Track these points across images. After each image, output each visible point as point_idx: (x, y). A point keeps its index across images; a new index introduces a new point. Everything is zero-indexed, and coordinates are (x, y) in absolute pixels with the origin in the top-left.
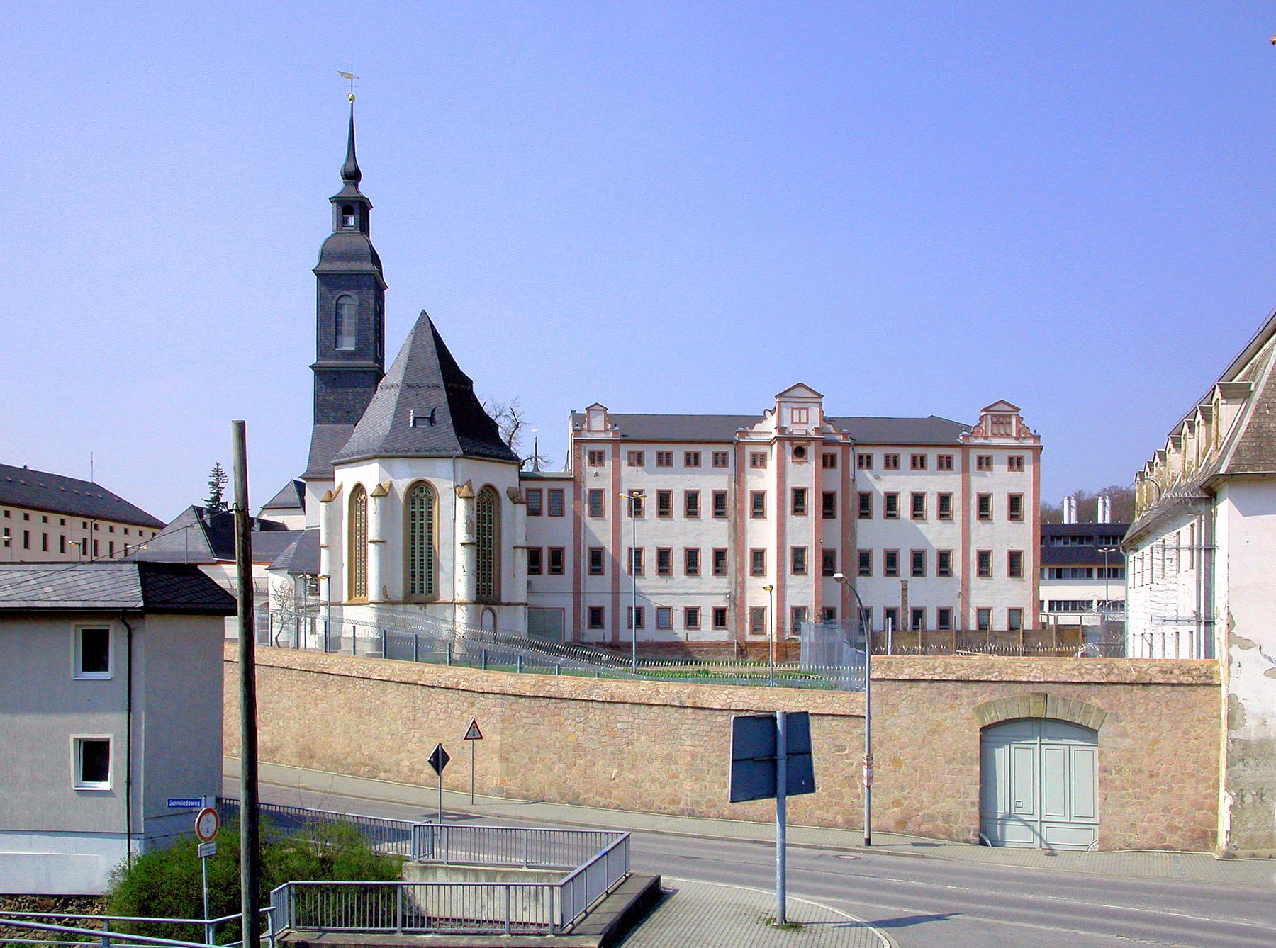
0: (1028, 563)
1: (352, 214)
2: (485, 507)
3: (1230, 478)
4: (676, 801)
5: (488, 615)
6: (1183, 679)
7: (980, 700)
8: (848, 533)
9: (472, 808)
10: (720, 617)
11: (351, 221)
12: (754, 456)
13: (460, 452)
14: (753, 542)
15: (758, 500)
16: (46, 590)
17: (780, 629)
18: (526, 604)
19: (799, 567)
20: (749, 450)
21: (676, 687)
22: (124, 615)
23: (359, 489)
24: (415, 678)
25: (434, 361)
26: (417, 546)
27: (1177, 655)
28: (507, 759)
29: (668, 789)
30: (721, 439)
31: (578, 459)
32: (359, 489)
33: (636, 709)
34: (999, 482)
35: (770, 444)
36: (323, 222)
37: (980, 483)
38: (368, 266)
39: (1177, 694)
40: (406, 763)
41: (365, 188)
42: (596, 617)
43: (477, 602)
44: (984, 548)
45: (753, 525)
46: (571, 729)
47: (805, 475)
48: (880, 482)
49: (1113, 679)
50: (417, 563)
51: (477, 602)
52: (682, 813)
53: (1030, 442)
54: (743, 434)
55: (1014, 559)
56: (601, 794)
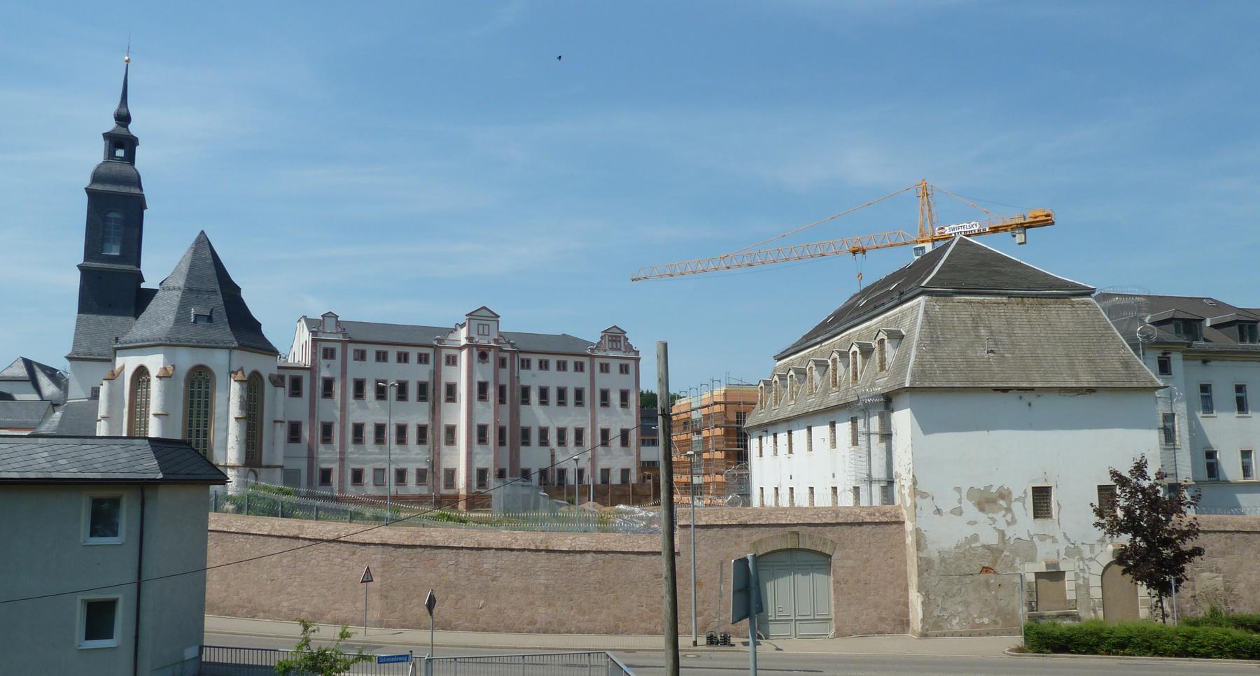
0: (633, 437)
3: (911, 390)
4: (532, 622)
5: (252, 474)
6: (884, 519)
7: (755, 538)
8: (515, 415)
9: (367, 639)
10: (421, 476)
11: (120, 153)
12: (448, 357)
13: (236, 344)
14: (447, 420)
15: (451, 391)
17: (469, 485)
18: (282, 467)
20: (444, 353)
22: (143, 486)
23: (141, 372)
24: (295, 532)
25: (212, 271)
28: (386, 597)
29: (526, 614)
31: (314, 354)
32: (141, 372)
33: (500, 553)
34: (614, 382)
36: (96, 154)
37: (602, 381)
40: (285, 604)
41: (133, 128)
42: (326, 476)
44: (604, 427)
45: (323, 403)
47: (485, 372)
48: (533, 378)
49: (840, 520)
50: (194, 433)
51: (245, 465)
52: (538, 631)
53: (632, 355)
54: (439, 341)
55: (625, 434)
56: (470, 621)
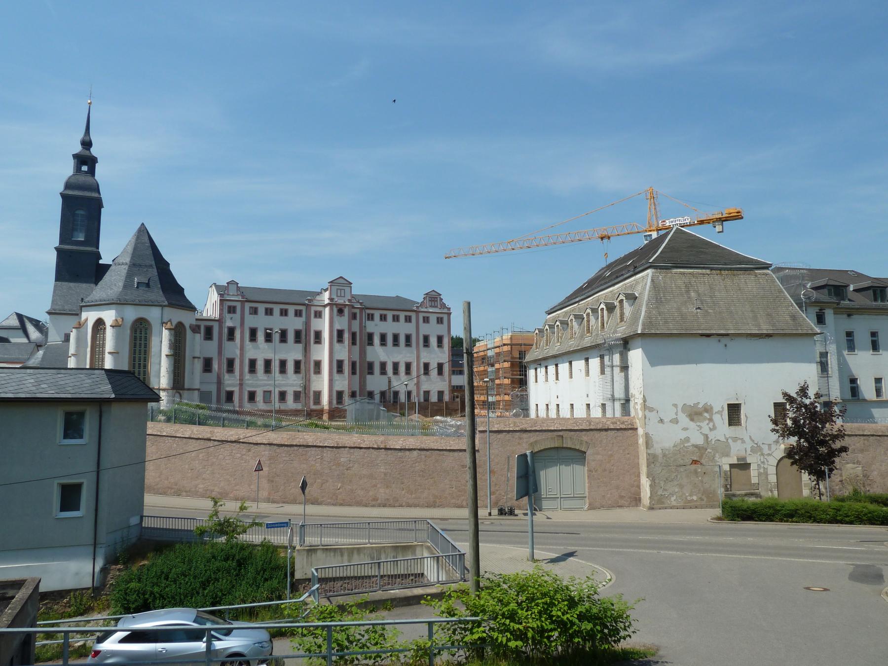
0: (446, 369)
1: (86, 164)
2: (178, 332)
5: (177, 395)
7: (532, 440)
8: (363, 353)
9: (258, 511)
11: (85, 168)
12: (316, 312)
13: (166, 303)
15: (318, 336)
16: (43, 386)
17: (330, 402)
18: (198, 390)
19: (340, 370)
20: (313, 309)
21: (373, 438)
22: (100, 403)
25: (149, 252)
26: (137, 356)
27: (547, 415)
28: (272, 481)
29: (371, 493)
30: (302, 304)
31: (221, 310)
33: (352, 450)
35: (325, 306)
36: (67, 169)
37: (425, 329)
38: (96, 195)
39: (620, 433)
40: (201, 486)
41: (94, 151)
42: (230, 396)
43: (173, 388)
46: (313, 463)
48: (376, 327)
51: (173, 388)
52: (379, 506)
53: (445, 311)
55: (440, 367)
